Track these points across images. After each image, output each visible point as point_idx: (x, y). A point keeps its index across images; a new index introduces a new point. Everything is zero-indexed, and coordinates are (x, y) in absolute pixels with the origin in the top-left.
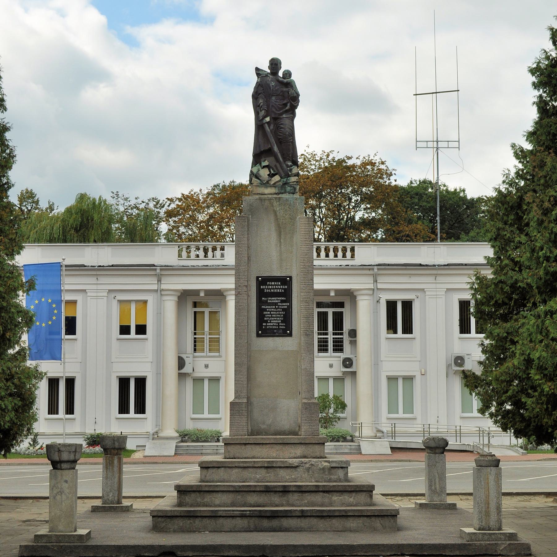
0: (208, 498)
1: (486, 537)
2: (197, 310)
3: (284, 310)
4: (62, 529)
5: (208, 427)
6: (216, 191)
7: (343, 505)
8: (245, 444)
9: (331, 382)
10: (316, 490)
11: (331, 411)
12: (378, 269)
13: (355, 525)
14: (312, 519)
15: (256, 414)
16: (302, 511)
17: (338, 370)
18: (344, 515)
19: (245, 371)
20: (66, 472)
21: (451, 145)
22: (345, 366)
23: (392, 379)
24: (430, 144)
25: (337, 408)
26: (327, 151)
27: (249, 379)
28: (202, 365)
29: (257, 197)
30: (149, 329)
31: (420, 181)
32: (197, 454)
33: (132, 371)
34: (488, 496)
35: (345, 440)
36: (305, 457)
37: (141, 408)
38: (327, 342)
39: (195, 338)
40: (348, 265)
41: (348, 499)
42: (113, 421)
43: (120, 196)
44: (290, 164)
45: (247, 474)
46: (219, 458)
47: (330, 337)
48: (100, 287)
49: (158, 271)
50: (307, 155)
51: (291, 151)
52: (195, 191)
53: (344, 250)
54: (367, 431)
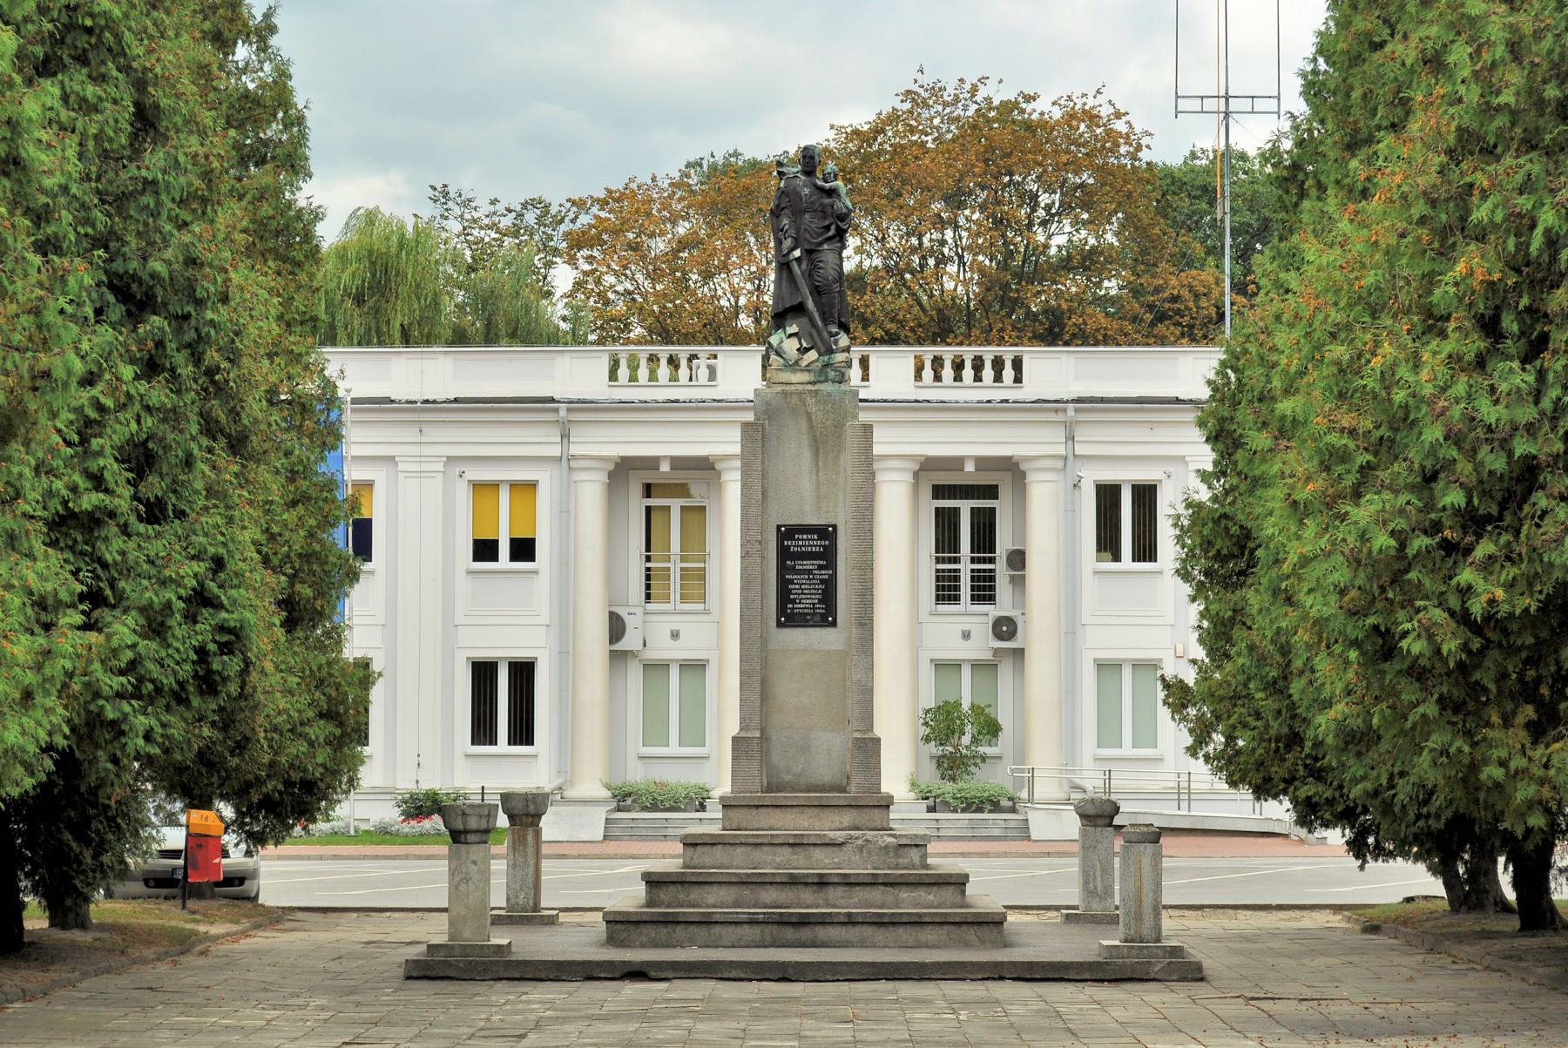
0: (696, 894)
1: (1134, 952)
2: (652, 502)
3: (823, 581)
4: (469, 936)
5: (679, 777)
6: (694, 180)
7: (916, 906)
8: (757, 807)
9: (966, 672)
10: (873, 882)
11: (966, 740)
12: (1076, 410)
13: (935, 937)
14: (865, 927)
15: (776, 756)
16: (849, 914)
17: (982, 645)
18: (917, 922)
19: (757, 686)
20: (476, 847)
21: (1260, 105)
22: (999, 636)
23: (1108, 668)
24: (1210, 104)
25: (979, 733)
26: (971, 79)
27: (764, 698)
28: (664, 632)
29: (779, 388)
30: (541, 549)
31: (1215, 151)
32: (655, 838)
33: (504, 647)
34: (1139, 890)
35: (996, 807)
36: (857, 829)
37: (523, 732)
38: (957, 579)
39: (648, 569)
40: (1007, 401)
41: (923, 895)
42: (460, 762)
43: (452, 195)
44: (835, 330)
45: (758, 855)
46: (715, 829)
47: (965, 568)
48: (427, 450)
49: (563, 413)
50: (921, 91)
51: (838, 307)
52: (639, 181)
53: (998, 364)
54: (1046, 788)
